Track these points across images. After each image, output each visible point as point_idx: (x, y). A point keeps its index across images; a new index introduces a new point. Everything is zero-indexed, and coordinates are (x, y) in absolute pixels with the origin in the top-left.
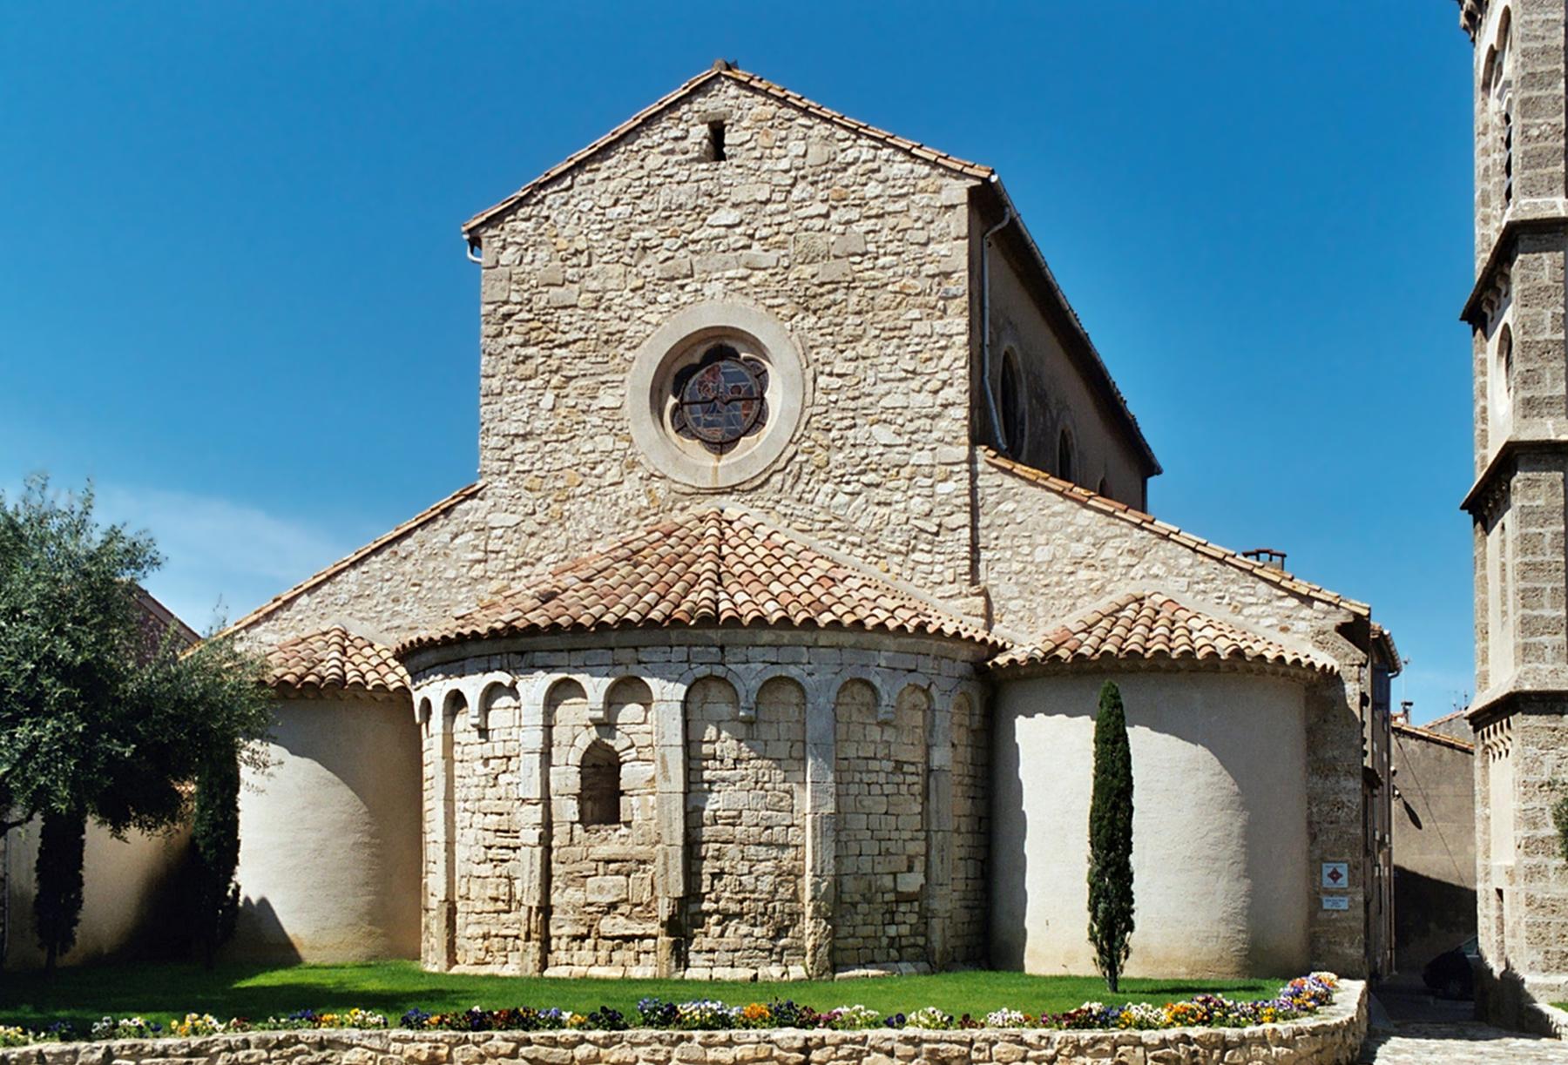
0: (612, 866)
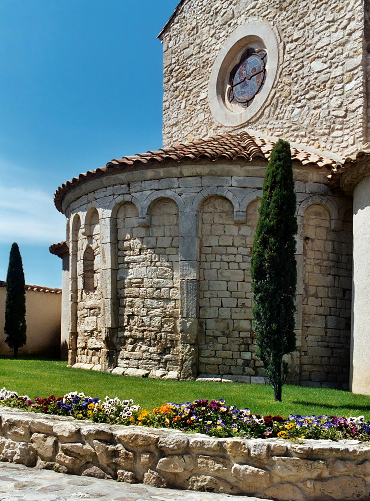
0: (92, 311)
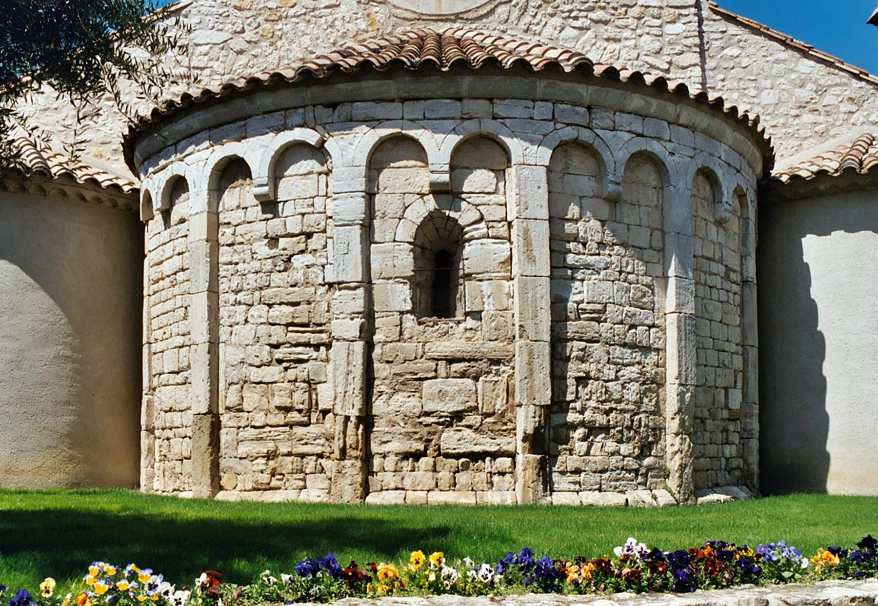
0: (456, 367)
